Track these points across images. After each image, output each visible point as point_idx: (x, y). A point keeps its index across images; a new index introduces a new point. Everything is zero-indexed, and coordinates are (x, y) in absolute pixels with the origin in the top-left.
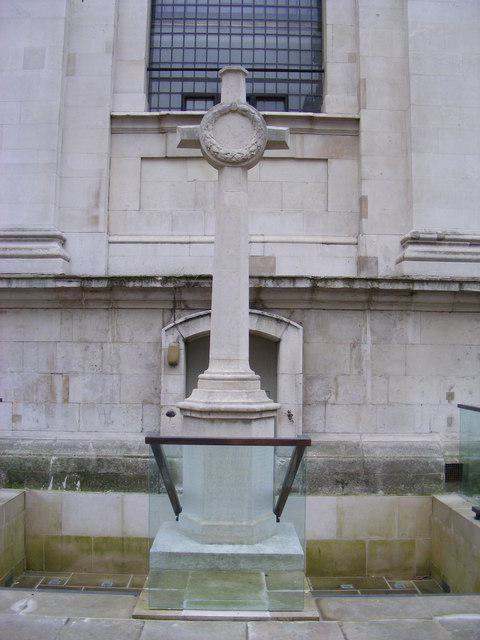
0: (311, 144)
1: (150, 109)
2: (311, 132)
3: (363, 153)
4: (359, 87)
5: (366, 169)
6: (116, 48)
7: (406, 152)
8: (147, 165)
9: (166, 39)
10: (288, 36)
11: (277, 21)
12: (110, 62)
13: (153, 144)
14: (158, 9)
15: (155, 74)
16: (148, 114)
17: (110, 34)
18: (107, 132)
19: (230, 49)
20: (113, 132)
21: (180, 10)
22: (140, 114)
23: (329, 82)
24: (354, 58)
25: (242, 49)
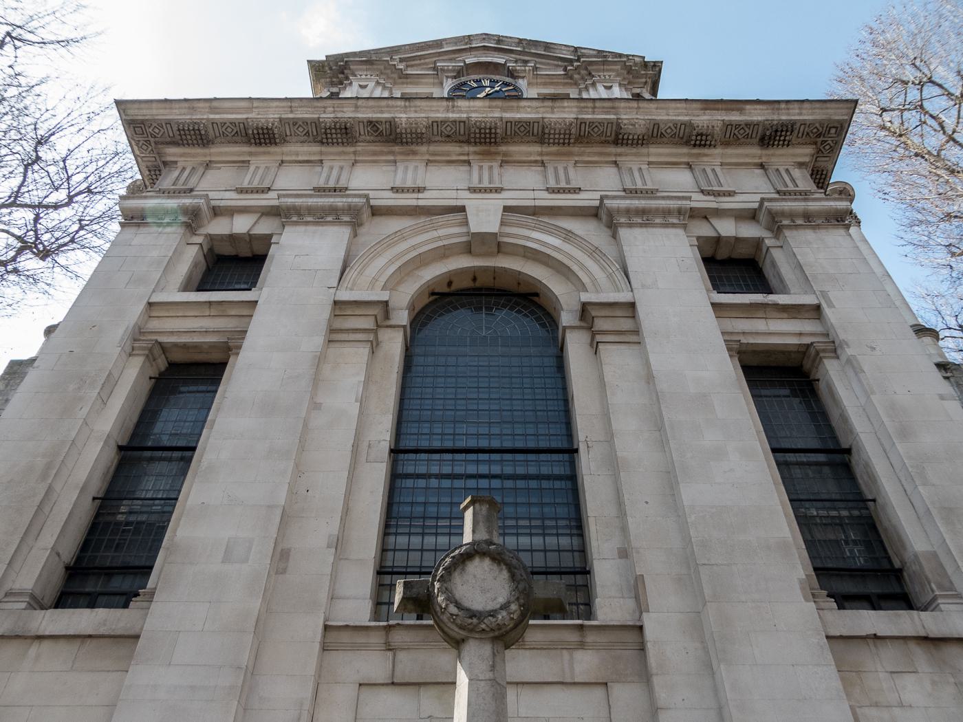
0: (585, 663)
1: (376, 620)
2: (582, 645)
3: (654, 671)
4: (637, 589)
5: (662, 695)
6: (339, 544)
7: (708, 668)
8: (366, 692)
9: (402, 541)
10: (544, 535)
11: (530, 519)
12: (331, 559)
13: (373, 664)
14: (405, 413)
15: (458, 123)
16: (373, 624)
17: (334, 527)
18: (317, 647)
19: (436, 550)
20: (325, 648)
21: (420, 509)
22: (363, 624)
23: (598, 583)
24: (624, 553)
25: (408, 550)
